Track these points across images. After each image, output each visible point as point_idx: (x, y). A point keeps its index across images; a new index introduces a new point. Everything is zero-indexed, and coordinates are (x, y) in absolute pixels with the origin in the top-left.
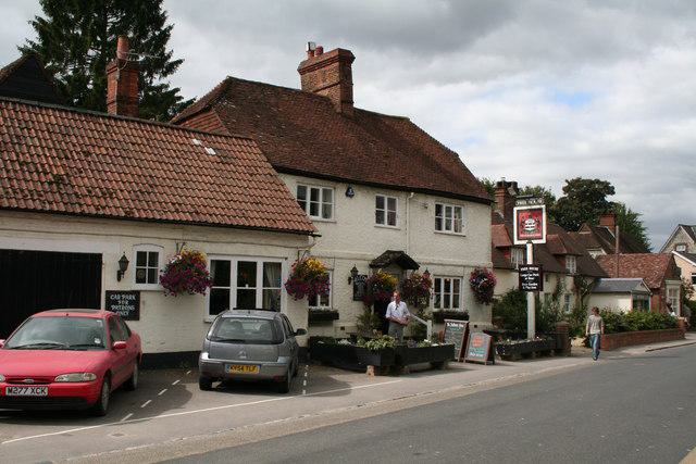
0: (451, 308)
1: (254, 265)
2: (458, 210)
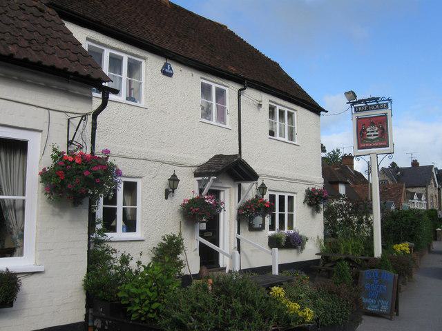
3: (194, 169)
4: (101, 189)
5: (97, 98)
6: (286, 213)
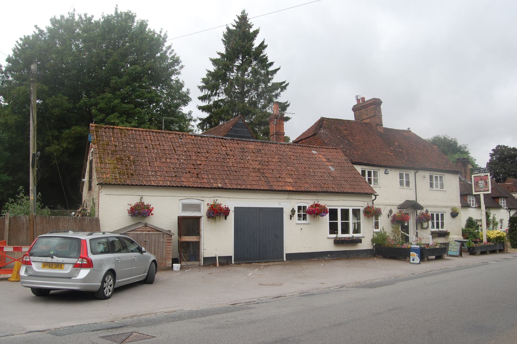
0: (440, 229)
2: (441, 177)
3: (398, 206)
4: (368, 214)
5: (373, 197)
6: (440, 221)
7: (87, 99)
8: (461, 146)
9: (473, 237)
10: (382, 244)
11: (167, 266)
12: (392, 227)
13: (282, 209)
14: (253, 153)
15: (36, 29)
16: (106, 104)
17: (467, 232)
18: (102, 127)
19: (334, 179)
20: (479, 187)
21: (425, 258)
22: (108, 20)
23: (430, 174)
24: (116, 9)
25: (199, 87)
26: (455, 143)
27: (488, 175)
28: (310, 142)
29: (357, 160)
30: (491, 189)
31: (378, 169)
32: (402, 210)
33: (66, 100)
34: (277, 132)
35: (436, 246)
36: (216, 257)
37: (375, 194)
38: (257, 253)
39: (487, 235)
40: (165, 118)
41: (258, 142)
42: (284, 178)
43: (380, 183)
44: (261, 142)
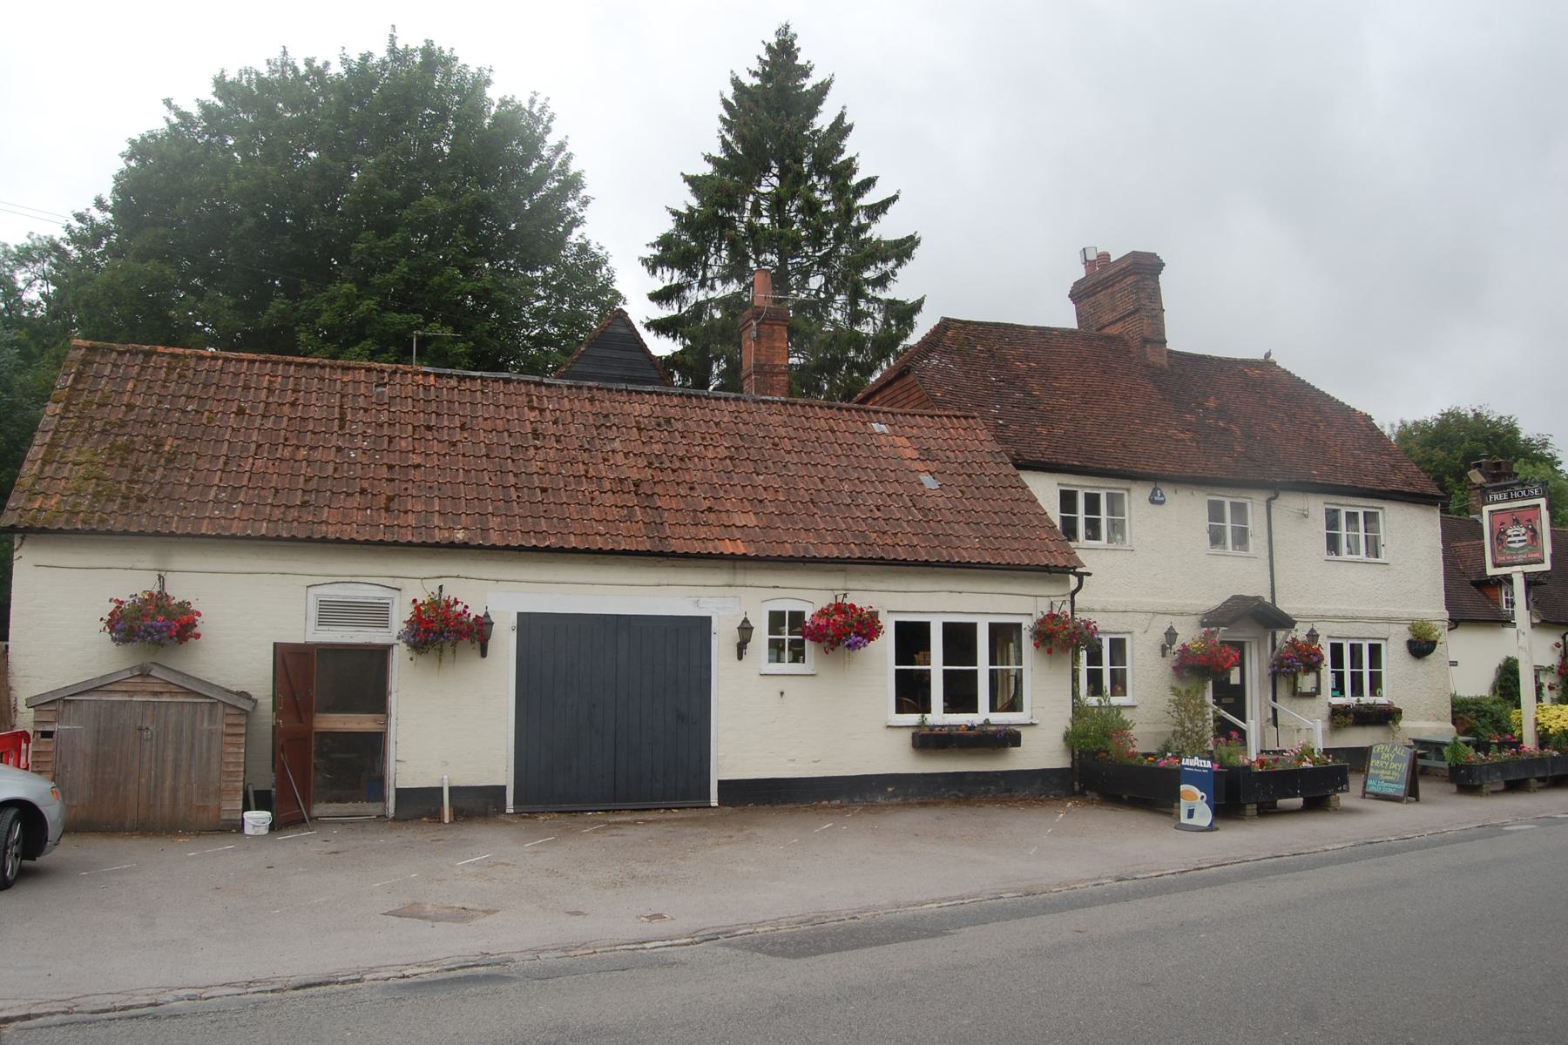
0: (1367, 699)
1: (972, 628)
3: (1200, 617)
5: (1073, 580)
6: (1366, 670)
7: (286, 301)
8: (1530, 440)
9: (1490, 728)
10: (1100, 751)
11: (225, 817)
12: (1173, 689)
13: (707, 621)
14: (639, 429)
15: (167, 108)
16: (340, 315)
17: (1469, 711)
18: (112, 350)
19: (925, 516)
20: (1509, 547)
21: (1248, 807)
22: (362, 74)
23: (1325, 503)
24: (393, 39)
25: (645, 261)
26: (1510, 432)
27: (1538, 506)
28: (895, 400)
29: (1041, 455)
30: (1552, 556)
31: (1124, 486)
32: (1213, 629)
33: (229, 308)
34: (762, 366)
35: (1301, 760)
36: (441, 789)
37: (1078, 570)
38: (603, 776)
39: (1536, 719)
40: (420, 333)
41: (673, 394)
42: (727, 511)
43: (1131, 536)
44: (681, 395)
